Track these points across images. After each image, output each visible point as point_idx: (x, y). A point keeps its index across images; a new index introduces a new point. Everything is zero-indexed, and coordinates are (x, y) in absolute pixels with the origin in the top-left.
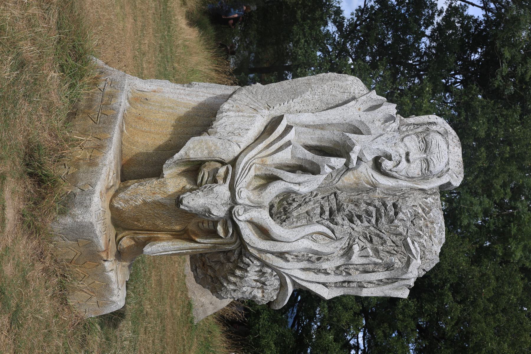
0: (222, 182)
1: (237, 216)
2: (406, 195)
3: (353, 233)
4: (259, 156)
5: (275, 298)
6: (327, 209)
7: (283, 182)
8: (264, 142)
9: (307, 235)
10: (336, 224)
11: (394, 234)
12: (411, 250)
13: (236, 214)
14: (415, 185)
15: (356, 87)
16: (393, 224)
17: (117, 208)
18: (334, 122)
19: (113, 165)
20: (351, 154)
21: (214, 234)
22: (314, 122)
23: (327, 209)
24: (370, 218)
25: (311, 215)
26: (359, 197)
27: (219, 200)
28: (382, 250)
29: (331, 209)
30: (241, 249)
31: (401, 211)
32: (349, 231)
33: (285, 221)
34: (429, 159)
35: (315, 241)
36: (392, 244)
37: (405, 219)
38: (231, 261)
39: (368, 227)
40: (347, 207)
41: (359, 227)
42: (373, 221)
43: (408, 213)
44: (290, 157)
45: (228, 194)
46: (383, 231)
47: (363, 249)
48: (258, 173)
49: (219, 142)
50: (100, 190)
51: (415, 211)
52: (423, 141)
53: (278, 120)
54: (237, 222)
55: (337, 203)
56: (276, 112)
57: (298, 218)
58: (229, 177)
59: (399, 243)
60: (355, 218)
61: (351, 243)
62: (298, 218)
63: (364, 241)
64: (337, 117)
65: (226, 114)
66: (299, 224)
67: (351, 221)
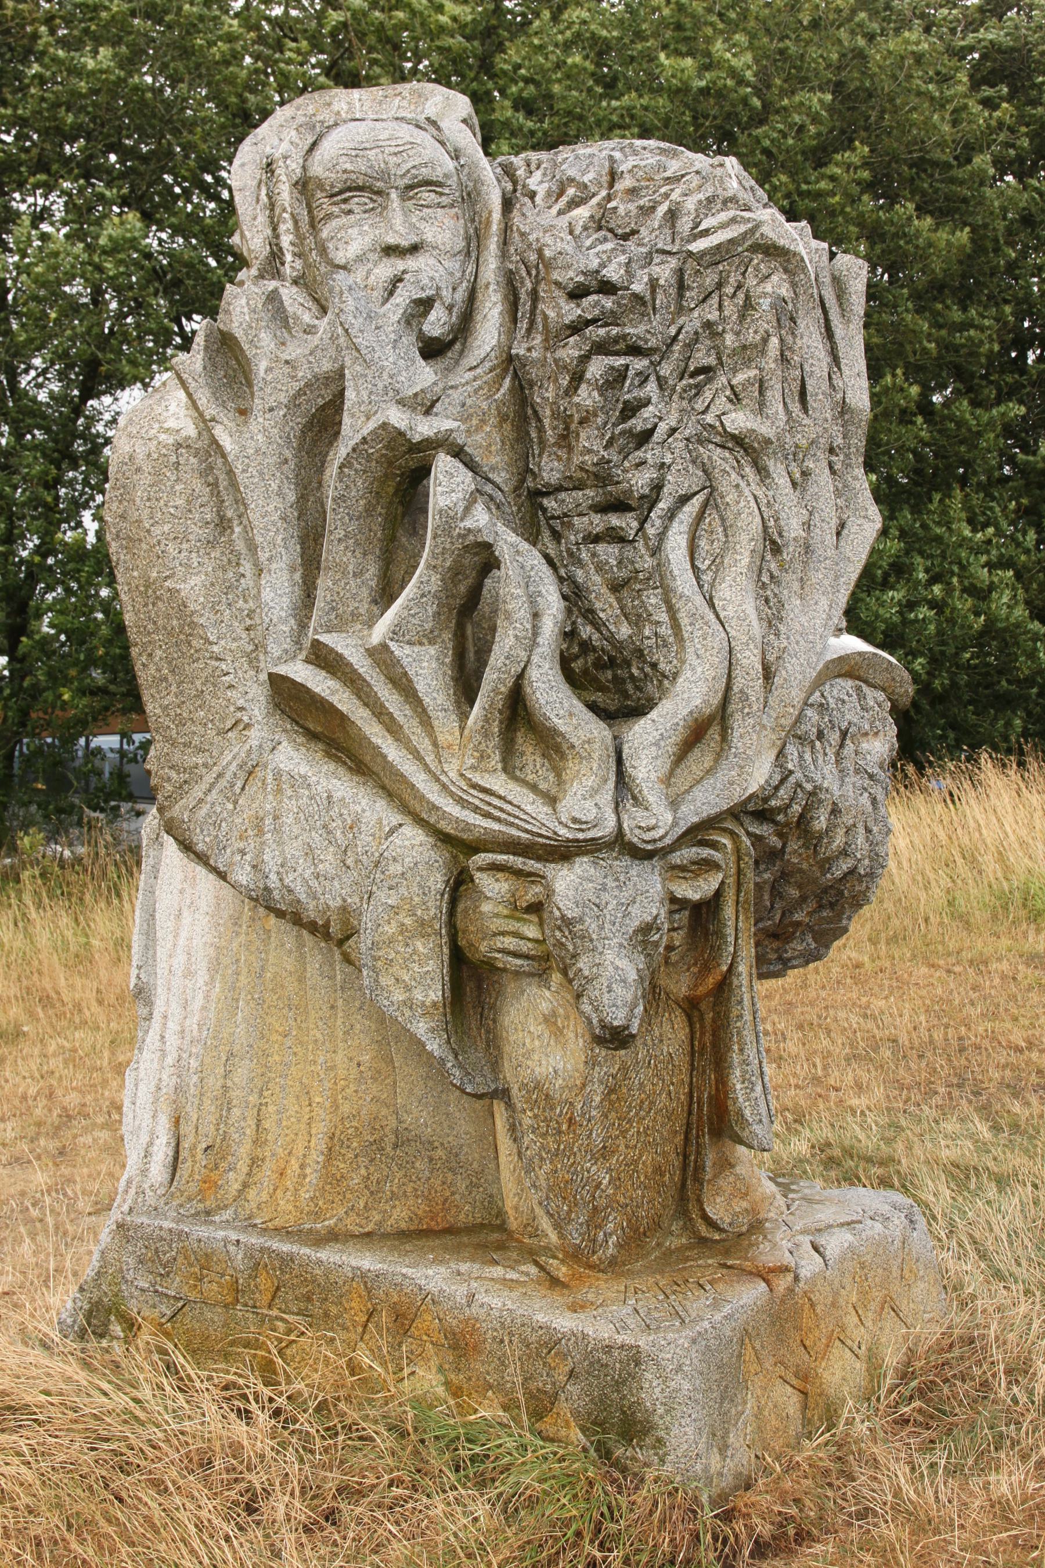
0: (538, 889)
1: (661, 832)
2: (533, 257)
3: (687, 432)
4: (429, 759)
5: (881, 696)
6: (598, 522)
7: (533, 673)
8: (377, 740)
9: (701, 587)
10: (657, 487)
11: (681, 296)
12: (731, 241)
13: (648, 836)
14: (494, 227)
15: (156, 426)
16: (648, 297)
17: (619, 1246)
18: (292, 497)
19: (464, 1267)
20: (417, 438)
21: (711, 906)
22: (292, 569)
23: (598, 522)
24: (631, 373)
25: (624, 574)
26: (548, 413)
27: (606, 897)
28: (737, 334)
29: (603, 509)
30: (746, 813)
31: (597, 272)
32: (682, 445)
33: (654, 666)
34: (407, 181)
35: (717, 563)
36: (714, 300)
37: (623, 259)
38: (779, 845)
39: (661, 382)
40: (590, 451)
41: (659, 412)
42: (639, 364)
43: (600, 248)
44: (432, 651)
45: (582, 865)
46: (673, 331)
47: (736, 398)
48: (495, 760)
49: (386, 897)
50: (568, 1314)
51: (585, 228)
52: (345, 201)
53: (287, 697)
54: (680, 831)
55: (575, 488)
56: (254, 700)
57: (637, 620)
58: (517, 862)
59: (710, 279)
60: (638, 424)
61: (718, 439)
62: (637, 620)
63: (708, 394)
64: (274, 486)
65: (273, 877)
66: (664, 617)
67: (645, 437)
